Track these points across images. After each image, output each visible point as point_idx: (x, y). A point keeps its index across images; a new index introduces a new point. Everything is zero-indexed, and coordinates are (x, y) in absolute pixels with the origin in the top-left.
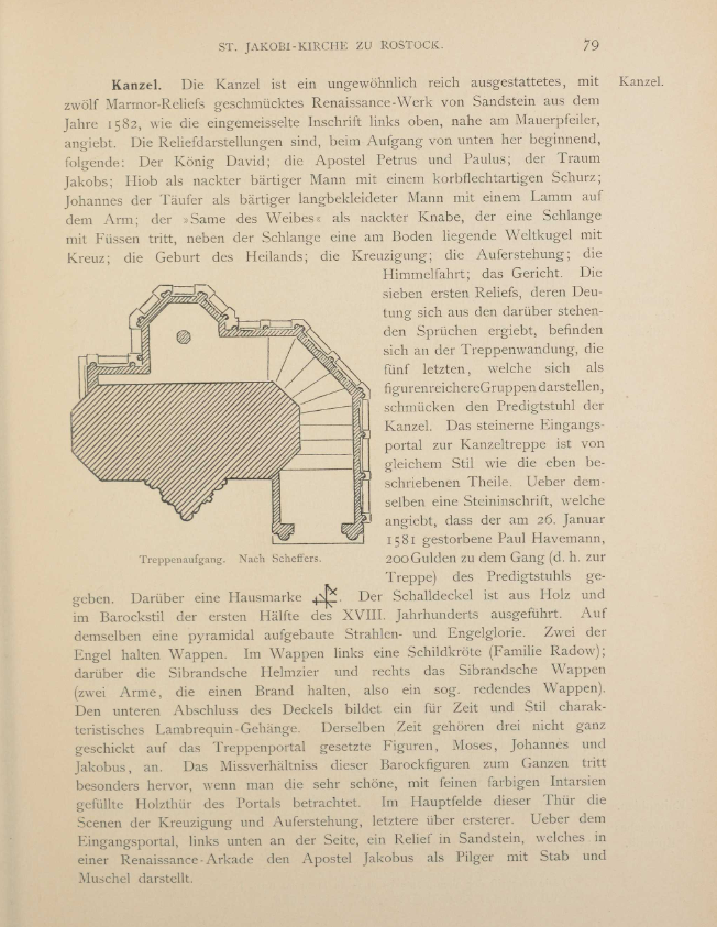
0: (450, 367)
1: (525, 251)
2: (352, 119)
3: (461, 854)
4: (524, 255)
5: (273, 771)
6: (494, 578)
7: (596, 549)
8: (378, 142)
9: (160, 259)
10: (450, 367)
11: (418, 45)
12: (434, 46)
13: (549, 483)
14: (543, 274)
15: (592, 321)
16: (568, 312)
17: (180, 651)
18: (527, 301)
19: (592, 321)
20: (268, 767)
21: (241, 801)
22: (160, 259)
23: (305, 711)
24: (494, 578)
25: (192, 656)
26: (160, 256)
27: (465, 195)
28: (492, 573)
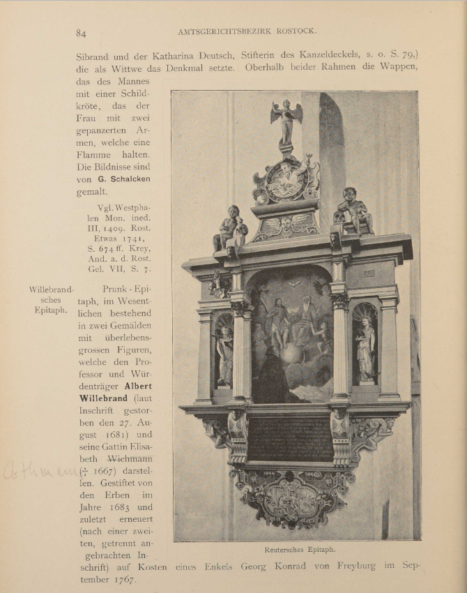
0: (117, 129)
1: (127, 311)
2: (122, 481)
3: (106, 287)
4: (126, 314)
5: (269, 71)
6: (107, 290)
7: (83, 101)
8: (144, 423)
9: (104, 484)
10: (117, 129)
11: (300, 31)
12: (311, 31)
13: (133, 338)
14: (95, 532)
15: (145, 320)
16: (92, 107)
17: (138, 372)
18: (120, 476)
19: (145, 320)
20: (266, 68)
21: (138, 360)
22: (105, 448)
23: (340, 55)
24: (107, 290)
25: (395, 67)
26: (104, 483)
27: (86, 337)
28: (106, 287)
